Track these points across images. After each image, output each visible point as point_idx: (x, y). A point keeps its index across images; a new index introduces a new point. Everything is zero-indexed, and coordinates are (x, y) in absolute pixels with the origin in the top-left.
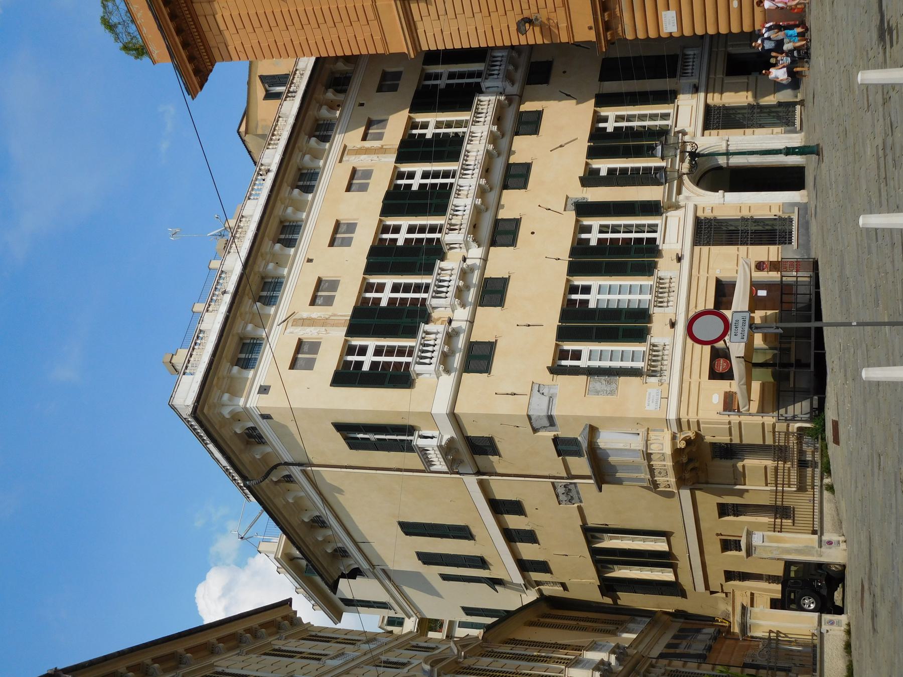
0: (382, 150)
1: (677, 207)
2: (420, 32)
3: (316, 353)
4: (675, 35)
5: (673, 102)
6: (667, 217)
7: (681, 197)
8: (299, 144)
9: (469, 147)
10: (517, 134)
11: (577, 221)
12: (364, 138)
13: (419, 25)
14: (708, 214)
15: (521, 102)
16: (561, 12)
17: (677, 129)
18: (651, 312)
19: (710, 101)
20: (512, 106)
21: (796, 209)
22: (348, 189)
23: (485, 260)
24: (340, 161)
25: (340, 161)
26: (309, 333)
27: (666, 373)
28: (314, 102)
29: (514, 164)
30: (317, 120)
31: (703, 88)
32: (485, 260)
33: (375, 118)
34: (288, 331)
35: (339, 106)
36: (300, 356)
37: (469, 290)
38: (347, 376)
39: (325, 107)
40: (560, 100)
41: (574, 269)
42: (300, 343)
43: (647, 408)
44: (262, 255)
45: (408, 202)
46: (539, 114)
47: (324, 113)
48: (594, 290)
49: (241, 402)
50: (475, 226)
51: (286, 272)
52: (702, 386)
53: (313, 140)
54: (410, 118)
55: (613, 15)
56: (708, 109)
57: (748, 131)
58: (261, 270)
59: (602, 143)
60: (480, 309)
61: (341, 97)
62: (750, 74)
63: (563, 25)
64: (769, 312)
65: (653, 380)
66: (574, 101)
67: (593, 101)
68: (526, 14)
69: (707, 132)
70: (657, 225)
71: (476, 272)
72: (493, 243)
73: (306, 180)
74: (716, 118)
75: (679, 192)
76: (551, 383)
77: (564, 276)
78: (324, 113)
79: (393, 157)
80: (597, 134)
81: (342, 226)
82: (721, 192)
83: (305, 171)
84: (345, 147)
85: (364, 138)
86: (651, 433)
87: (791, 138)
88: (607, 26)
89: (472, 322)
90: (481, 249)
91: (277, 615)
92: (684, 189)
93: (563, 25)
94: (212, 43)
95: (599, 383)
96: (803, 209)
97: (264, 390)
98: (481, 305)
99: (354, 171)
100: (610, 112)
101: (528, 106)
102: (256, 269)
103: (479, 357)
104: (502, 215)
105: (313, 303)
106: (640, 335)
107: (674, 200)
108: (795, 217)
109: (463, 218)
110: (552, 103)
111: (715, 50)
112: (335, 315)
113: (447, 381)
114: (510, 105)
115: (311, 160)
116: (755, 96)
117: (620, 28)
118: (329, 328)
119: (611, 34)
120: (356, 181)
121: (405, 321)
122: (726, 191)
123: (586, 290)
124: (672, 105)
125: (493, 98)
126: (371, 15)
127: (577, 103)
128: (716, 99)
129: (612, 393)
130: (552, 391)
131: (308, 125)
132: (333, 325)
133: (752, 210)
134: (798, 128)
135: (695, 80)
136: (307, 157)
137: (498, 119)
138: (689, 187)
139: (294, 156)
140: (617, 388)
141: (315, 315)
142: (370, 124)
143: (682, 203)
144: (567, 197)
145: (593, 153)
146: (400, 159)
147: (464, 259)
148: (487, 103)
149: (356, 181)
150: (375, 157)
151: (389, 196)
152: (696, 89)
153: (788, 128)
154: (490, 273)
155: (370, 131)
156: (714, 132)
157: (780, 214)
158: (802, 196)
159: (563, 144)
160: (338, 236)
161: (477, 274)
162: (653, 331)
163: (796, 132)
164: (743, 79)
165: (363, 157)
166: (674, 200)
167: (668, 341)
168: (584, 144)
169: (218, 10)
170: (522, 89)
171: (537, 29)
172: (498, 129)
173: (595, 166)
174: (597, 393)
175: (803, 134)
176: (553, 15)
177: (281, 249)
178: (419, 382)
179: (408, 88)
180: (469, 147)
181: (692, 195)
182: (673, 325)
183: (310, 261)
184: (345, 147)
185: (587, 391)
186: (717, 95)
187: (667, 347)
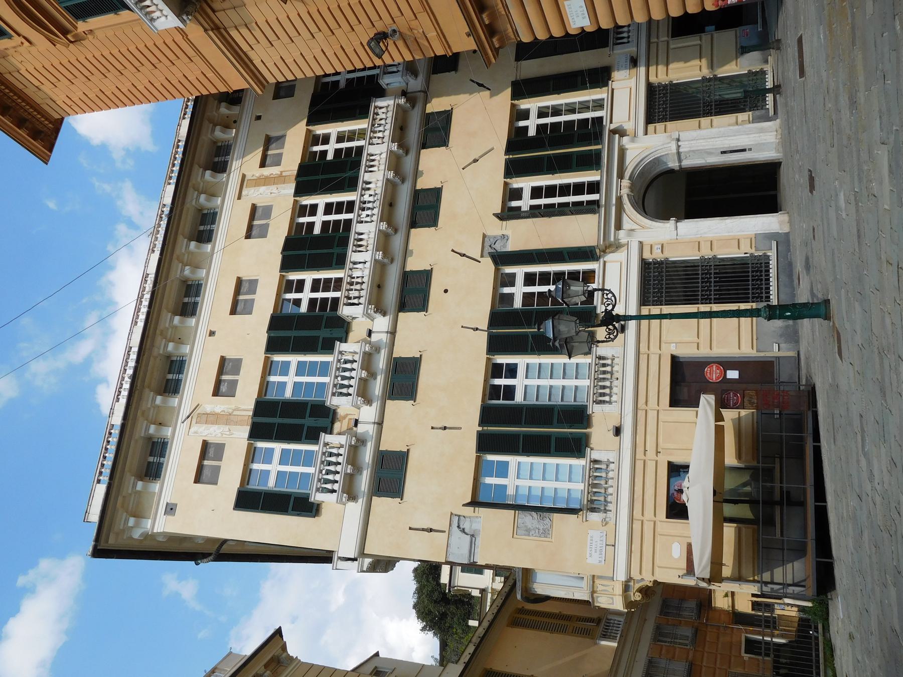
0: (279, 179)
1: (616, 246)
2: (257, 62)
3: (220, 459)
4: (588, 30)
5: (606, 85)
6: (605, 263)
7: (622, 233)
8: (193, 182)
9: (367, 177)
10: (424, 146)
11: (497, 270)
12: (263, 165)
13: (251, 54)
14: (658, 255)
15: (426, 101)
16: (424, 18)
17: (613, 126)
18: (590, 412)
19: (653, 79)
20: (416, 109)
21: (774, 244)
22: (248, 236)
23: (393, 333)
24: (239, 198)
25: (239, 198)
26: (214, 433)
27: (611, 507)
28: (206, 123)
29: (422, 190)
30: (215, 143)
31: (642, 60)
32: (393, 333)
33: (273, 134)
34: (192, 430)
35: (235, 122)
36: (206, 463)
37: (375, 378)
38: (249, 500)
39: (218, 128)
40: (471, 92)
41: (496, 345)
42: (205, 445)
43: (590, 561)
44: (161, 334)
45: (307, 252)
46: (446, 117)
47: (219, 134)
48: (521, 371)
49: (148, 524)
50: (379, 286)
51: (186, 349)
52: (658, 530)
53: (208, 173)
54: (309, 132)
55: (494, 16)
56: (651, 89)
57: (705, 121)
58: (161, 352)
59: (525, 152)
60: (390, 404)
61: (236, 110)
62: (703, 31)
63: (432, 34)
64: (744, 412)
65: (595, 517)
66: (488, 93)
67: (509, 91)
68: (380, 27)
69: (651, 127)
70: (593, 272)
71: (383, 352)
72: (403, 307)
73: (204, 228)
74: (665, 105)
75: (619, 227)
76: (472, 514)
77: (484, 356)
78: (219, 134)
79: (291, 188)
80: (517, 140)
81: (244, 283)
82: (672, 221)
83: (206, 212)
84: (244, 176)
85: (263, 165)
86: (597, 581)
87: (762, 131)
88: (491, 31)
89: (380, 424)
90: (387, 318)
91: (424, 306)
92: (625, 218)
93: (432, 34)
94: (39, 101)
95: (529, 520)
96: (783, 241)
97: (171, 509)
98: (390, 398)
99: (254, 208)
100: (532, 104)
101: (436, 105)
102: (155, 352)
103: (390, 475)
104: (413, 265)
105: (216, 393)
106: (575, 446)
107: (612, 239)
108: (772, 254)
109: (364, 273)
110: (462, 98)
111: (654, 40)
112: (237, 409)
113: (355, 509)
114: (413, 107)
115: (208, 200)
116: (711, 66)
117: (510, 30)
118: (233, 427)
119: (498, 40)
120: (253, 229)
121: (309, 422)
122: (679, 219)
123: (512, 371)
124: (605, 89)
125: (391, 102)
126: (191, 52)
127: (492, 96)
128: (662, 75)
129: (546, 533)
130: (475, 526)
131: (202, 153)
132: (236, 423)
133: (714, 247)
134: (771, 113)
135: (631, 49)
136: (203, 197)
137: (400, 131)
138: (632, 218)
139: (188, 200)
140: (551, 526)
141: (218, 409)
142: (269, 142)
143: (623, 241)
144: (484, 236)
145: (513, 169)
146: (300, 190)
147: (370, 333)
148: (385, 108)
149: (253, 229)
150: (273, 188)
151: (290, 244)
152: (634, 62)
153: (758, 113)
154: (403, 351)
155: (270, 152)
156: (660, 126)
157: (753, 251)
158: (781, 223)
159: (477, 157)
160: (241, 297)
161: (383, 354)
162: (594, 441)
163: (769, 119)
164: (692, 41)
165: (262, 189)
166: (612, 239)
167: (612, 457)
168: (499, 159)
169: (19, 66)
170: (428, 81)
171: (400, 44)
172: (400, 146)
173: (515, 186)
174: (528, 531)
175: (778, 121)
176: (414, 24)
177: (181, 322)
178: (324, 510)
179: (304, 98)
180: (367, 177)
181: (637, 227)
182: (618, 431)
183: (212, 333)
184: (244, 176)
185: (516, 528)
186: (661, 68)
187: (612, 466)
